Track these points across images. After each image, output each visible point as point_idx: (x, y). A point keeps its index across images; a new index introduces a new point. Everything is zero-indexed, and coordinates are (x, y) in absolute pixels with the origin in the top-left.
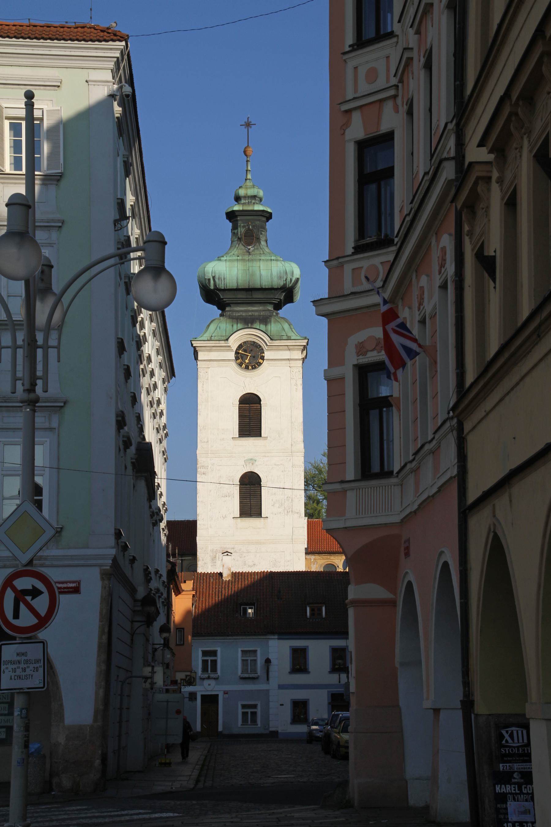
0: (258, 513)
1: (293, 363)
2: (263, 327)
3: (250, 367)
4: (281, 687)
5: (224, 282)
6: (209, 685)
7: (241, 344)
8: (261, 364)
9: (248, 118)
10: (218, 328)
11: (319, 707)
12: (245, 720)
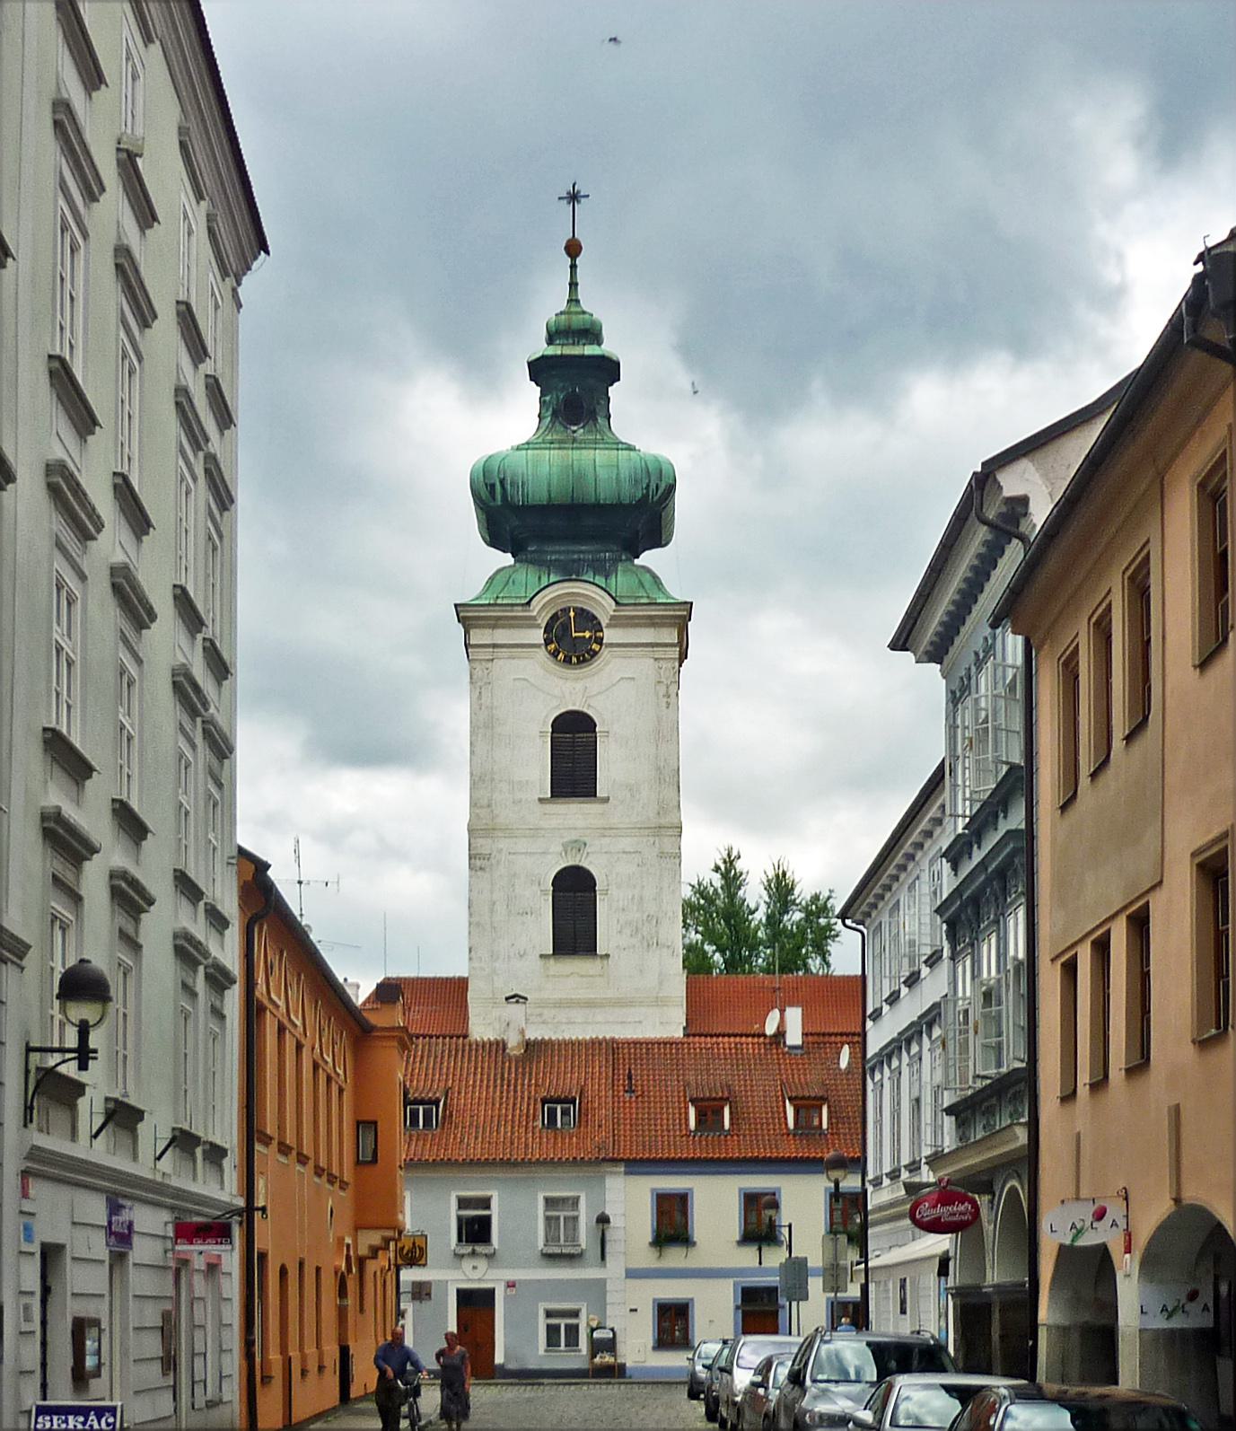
1: (659, 652)
2: (600, 580)
3: (561, 656)
4: (631, 1274)
6: (475, 1268)
7: (556, 614)
8: (596, 653)
12: (552, 1340)
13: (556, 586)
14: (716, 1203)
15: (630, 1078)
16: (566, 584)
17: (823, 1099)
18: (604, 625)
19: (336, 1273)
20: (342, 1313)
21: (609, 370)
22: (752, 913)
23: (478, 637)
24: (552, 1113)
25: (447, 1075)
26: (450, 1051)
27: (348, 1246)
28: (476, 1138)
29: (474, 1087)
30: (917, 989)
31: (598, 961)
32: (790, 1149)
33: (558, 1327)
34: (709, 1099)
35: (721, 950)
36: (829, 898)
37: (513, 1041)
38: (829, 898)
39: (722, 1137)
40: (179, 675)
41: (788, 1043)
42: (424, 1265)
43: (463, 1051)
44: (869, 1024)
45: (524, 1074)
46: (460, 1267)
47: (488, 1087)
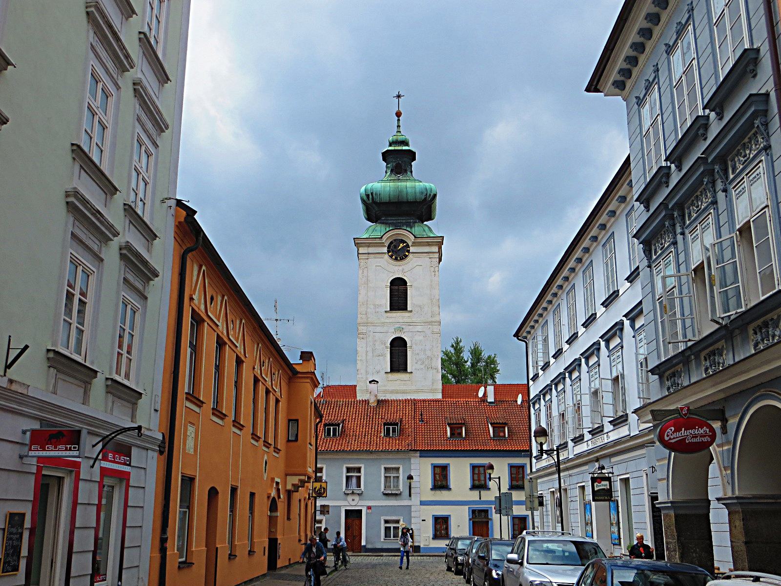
0: (404, 307)
1: (431, 255)
3: (394, 257)
4: (422, 503)
6: (353, 500)
8: (407, 256)
11: (460, 525)
12: (387, 535)
13: (392, 231)
14: (460, 471)
15: (421, 415)
16: (396, 230)
17: (506, 424)
18: (410, 245)
19: (268, 497)
20: (272, 521)
21: (412, 155)
22: (466, 362)
23: (362, 250)
24: (388, 430)
25: (344, 414)
26: (346, 404)
27: (277, 483)
28: (355, 441)
29: (355, 419)
30: (547, 371)
32: (492, 446)
33: (390, 528)
34: (456, 424)
35: (454, 377)
36: (495, 357)
37: (372, 400)
38: (495, 357)
39: (462, 441)
40: (91, 6)
41: (488, 401)
42: (325, 497)
43: (351, 404)
44: (531, 383)
45: (376, 414)
46: (346, 500)
47: (361, 419)
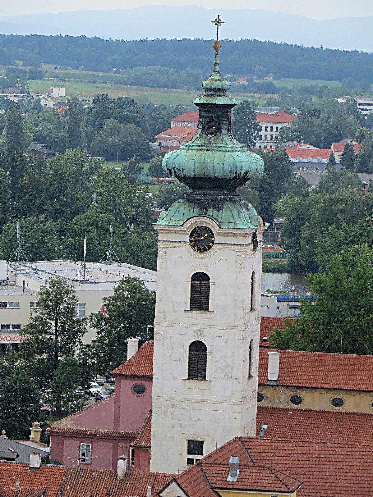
3: (196, 248)
5: (183, 172)
7: (194, 229)
9: (218, 16)
10: (177, 212)
31: (206, 383)
